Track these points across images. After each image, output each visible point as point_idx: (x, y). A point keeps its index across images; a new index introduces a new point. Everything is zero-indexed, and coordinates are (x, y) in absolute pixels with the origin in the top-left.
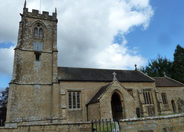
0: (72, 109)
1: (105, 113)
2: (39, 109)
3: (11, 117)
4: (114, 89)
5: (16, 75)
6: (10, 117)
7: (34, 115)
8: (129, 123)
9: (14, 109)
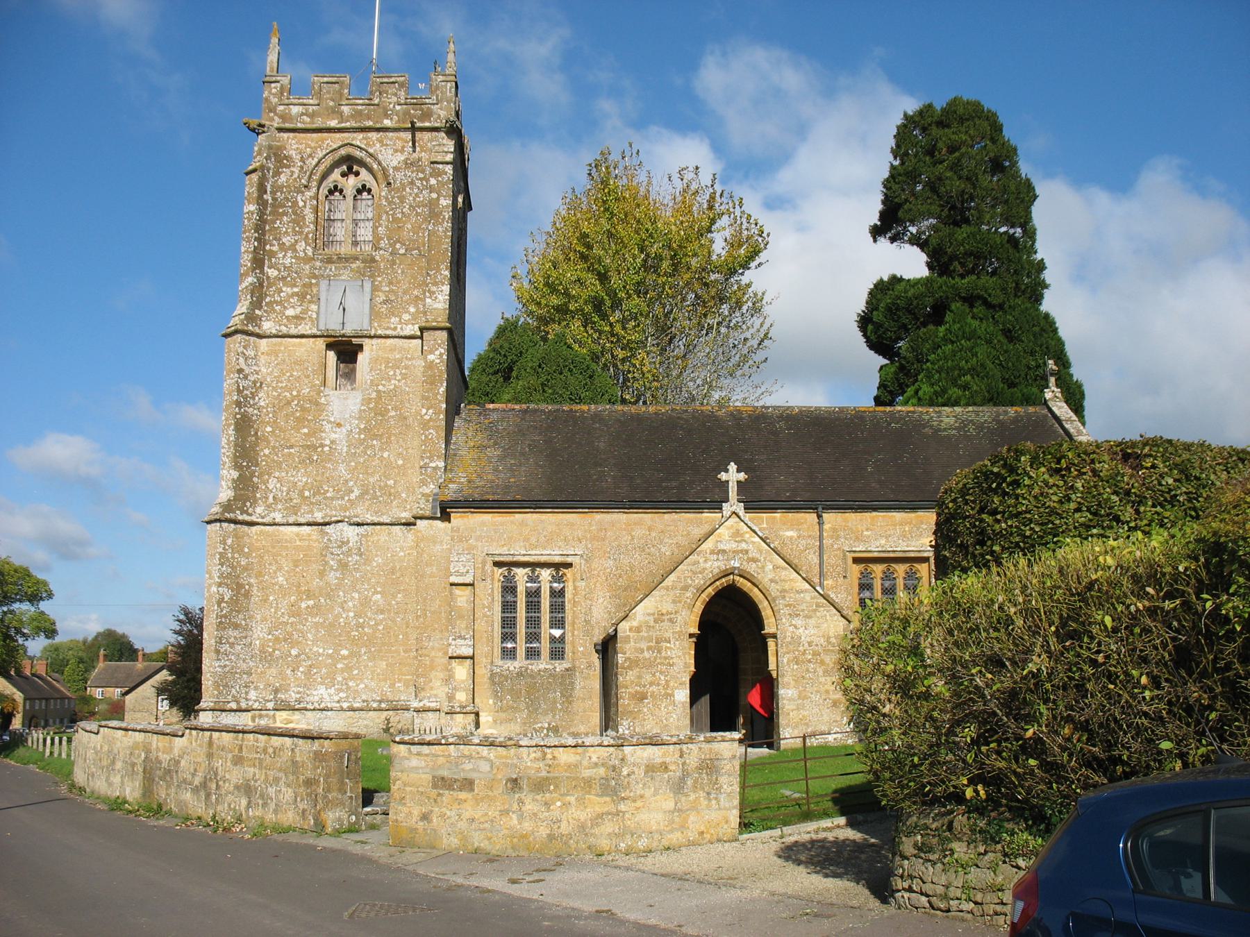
0: (520, 663)
1: (642, 697)
2: (352, 655)
3: (223, 683)
4: (714, 566)
5: (235, 474)
6: (216, 685)
7: (329, 681)
8: (414, 749)
9: (232, 645)
